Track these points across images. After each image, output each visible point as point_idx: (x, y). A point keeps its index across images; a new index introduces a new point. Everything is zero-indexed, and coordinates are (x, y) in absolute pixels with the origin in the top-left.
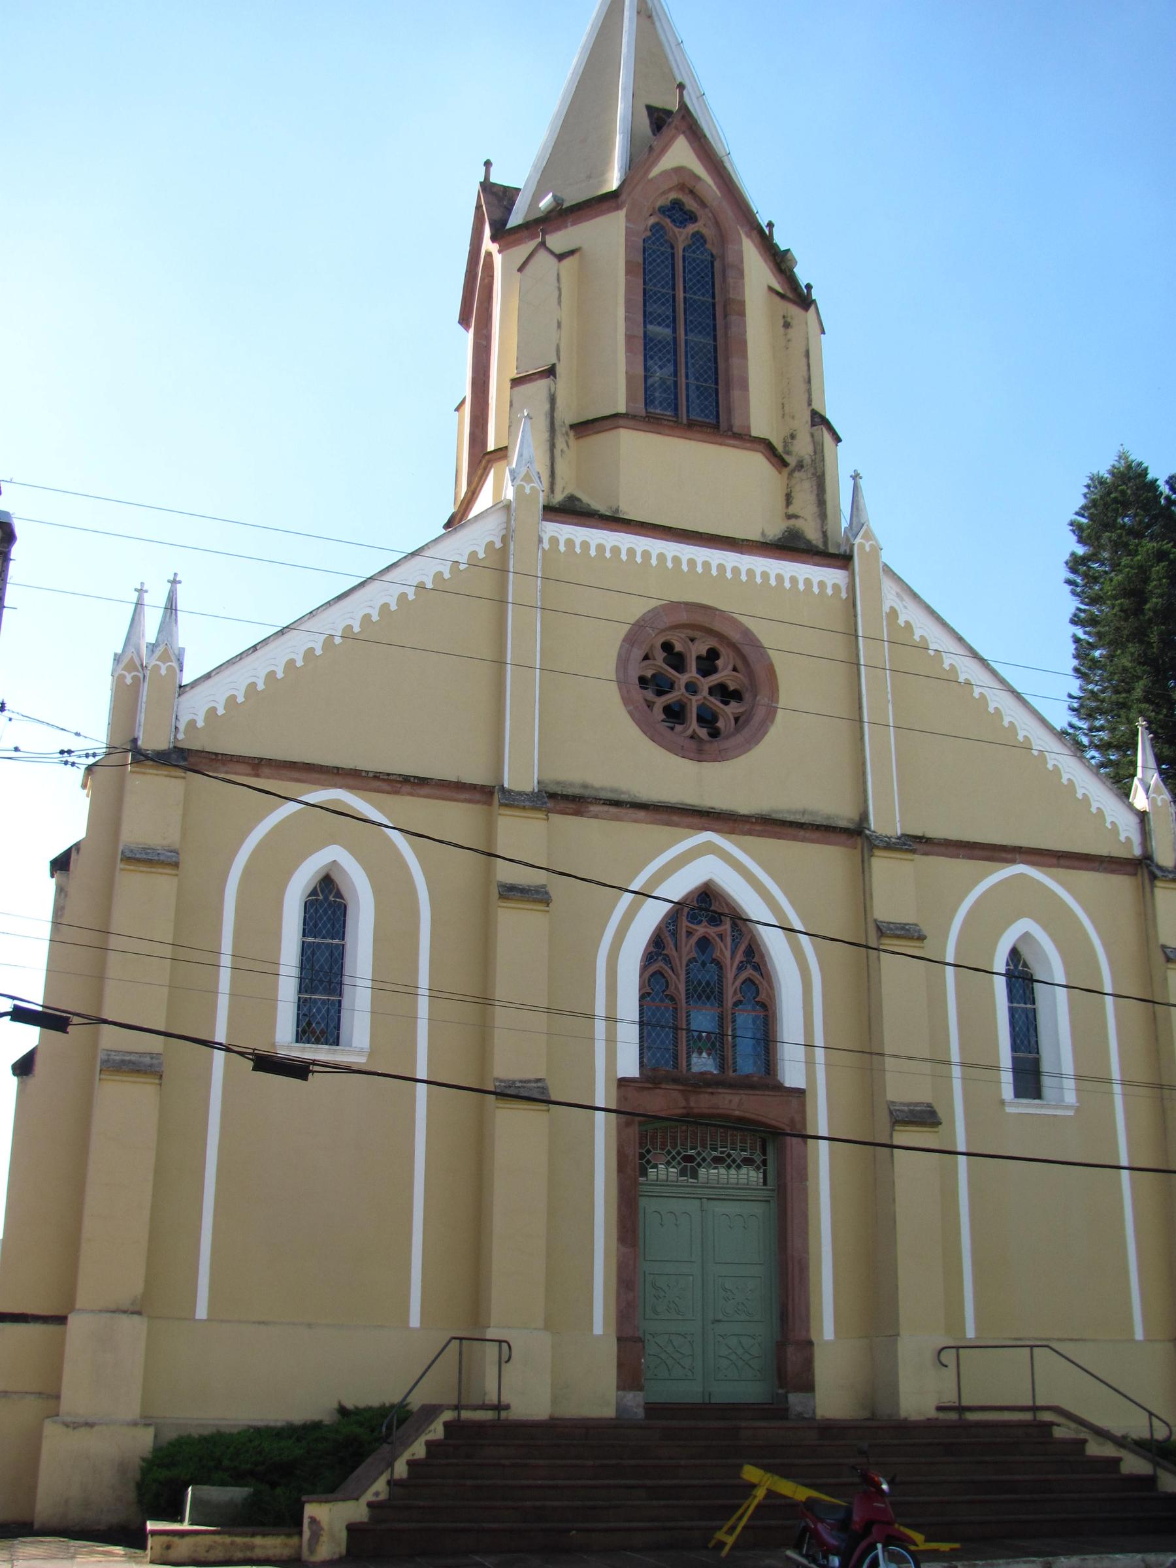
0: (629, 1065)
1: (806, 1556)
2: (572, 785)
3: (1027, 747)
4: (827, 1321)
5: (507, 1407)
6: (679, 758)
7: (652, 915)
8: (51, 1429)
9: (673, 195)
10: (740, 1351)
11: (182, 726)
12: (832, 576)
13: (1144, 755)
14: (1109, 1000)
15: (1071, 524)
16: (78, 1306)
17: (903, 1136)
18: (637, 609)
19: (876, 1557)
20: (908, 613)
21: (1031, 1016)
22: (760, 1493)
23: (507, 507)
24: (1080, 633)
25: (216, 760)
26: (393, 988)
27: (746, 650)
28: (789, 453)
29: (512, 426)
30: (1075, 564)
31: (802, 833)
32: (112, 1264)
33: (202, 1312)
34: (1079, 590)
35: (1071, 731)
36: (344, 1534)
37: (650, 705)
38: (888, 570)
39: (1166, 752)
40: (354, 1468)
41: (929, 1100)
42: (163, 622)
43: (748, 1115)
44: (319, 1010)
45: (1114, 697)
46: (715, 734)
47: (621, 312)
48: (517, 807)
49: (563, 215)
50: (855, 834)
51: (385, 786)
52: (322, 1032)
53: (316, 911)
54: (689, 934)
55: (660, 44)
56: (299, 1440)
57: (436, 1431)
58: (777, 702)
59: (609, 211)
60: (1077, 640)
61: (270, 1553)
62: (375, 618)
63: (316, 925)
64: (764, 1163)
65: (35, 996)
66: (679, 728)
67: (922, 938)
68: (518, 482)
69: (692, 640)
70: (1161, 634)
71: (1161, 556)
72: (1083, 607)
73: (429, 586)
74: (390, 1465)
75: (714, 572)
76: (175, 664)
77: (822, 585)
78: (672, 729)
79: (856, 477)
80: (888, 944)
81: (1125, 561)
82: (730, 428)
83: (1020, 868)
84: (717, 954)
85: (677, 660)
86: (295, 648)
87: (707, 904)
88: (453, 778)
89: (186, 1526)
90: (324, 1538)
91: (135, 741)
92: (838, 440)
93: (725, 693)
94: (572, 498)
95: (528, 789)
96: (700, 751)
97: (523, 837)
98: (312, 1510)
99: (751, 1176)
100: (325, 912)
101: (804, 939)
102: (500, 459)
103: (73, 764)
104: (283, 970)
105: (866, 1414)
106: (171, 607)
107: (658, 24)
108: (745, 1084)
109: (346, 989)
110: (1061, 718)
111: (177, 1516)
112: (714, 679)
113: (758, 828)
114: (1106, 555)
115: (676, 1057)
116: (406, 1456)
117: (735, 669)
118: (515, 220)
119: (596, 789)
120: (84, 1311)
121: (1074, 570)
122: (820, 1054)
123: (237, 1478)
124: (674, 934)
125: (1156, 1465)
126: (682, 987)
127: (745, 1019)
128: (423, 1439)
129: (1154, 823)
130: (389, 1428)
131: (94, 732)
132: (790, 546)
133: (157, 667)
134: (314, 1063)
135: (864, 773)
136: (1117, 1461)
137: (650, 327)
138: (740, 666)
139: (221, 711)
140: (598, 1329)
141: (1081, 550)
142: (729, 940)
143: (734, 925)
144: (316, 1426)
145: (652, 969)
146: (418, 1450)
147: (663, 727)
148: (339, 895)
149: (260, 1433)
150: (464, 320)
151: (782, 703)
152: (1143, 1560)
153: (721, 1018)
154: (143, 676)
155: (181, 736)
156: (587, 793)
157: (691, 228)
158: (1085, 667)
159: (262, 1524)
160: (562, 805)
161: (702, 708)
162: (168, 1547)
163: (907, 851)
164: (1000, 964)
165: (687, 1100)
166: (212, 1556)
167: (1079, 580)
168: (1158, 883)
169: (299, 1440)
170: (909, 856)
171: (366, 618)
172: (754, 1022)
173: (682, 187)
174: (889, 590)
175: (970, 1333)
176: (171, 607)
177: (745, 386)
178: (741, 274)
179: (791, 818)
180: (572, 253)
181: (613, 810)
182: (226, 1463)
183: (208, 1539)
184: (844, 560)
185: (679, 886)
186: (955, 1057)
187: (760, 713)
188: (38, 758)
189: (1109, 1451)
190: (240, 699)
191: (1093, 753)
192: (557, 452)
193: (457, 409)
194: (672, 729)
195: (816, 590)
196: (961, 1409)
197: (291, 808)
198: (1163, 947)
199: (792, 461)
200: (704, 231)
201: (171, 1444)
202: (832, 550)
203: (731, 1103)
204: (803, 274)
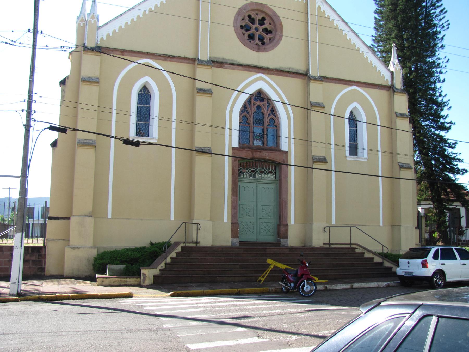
0: (236, 144)
1: (284, 284)
2: (219, 58)
4: (292, 219)
5: (199, 243)
6: (252, 51)
7: (243, 98)
8: (67, 249)
10: (267, 227)
11: (99, 39)
13: (394, 54)
14: (379, 127)
16: (74, 214)
17: (316, 166)
19: (304, 284)
21: (355, 131)
22: (272, 267)
24: (377, 16)
25: (110, 50)
26: (165, 119)
27: (274, 17)
31: (289, 74)
32: (83, 201)
33: (110, 216)
34: (377, 3)
35: (372, 47)
36: (153, 278)
39: (401, 54)
40: (155, 260)
41: (324, 155)
42: (92, 7)
43: (270, 159)
44: (143, 127)
45: (386, 37)
46: (263, 44)
48: (203, 65)
50: (305, 75)
51: (162, 58)
52: (144, 133)
53: (141, 96)
54: (254, 104)
56: (139, 252)
57: (179, 249)
60: (375, 18)
61: (132, 283)
62: (159, 6)
63: (141, 101)
64: (275, 173)
65: (57, 123)
66: (252, 41)
67: (324, 107)
70: (401, 17)
72: (378, 8)
74: (166, 259)
76: (96, 20)
78: (250, 42)
83: (354, 87)
84: (262, 110)
85: (252, 21)
87: (260, 96)
89: (107, 276)
90: (147, 279)
91: (84, 44)
93: (267, 31)
95: (206, 60)
96: (259, 49)
97: (204, 73)
98: (143, 271)
99: (271, 176)
100: (144, 97)
101: (289, 106)
103: (65, 51)
104: (132, 114)
105: (303, 245)
108: (270, 150)
109: (151, 120)
110: (369, 42)
111: (105, 273)
112: (264, 27)
113: (276, 73)
115: (249, 141)
116: (170, 256)
117: (270, 24)
119: (227, 60)
120: (75, 216)
122: (292, 141)
123: (122, 262)
124: (250, 104)
125: (383, 259)
126: (252, 120)
127: (271, 130)
128: (175, 251)
130: (165, 248)
131: (72, 41)
133: (90, 21)
134: (141, 142)
135: (308, 57)
136: (373, 258)
138: (272, 23)
139: (111, 35)
140: (226, 220)
142: (266, 107)
143: (268, 102)
144: (144, 248)
145: (243, 115)
146: (173, 254)
147: (248, 41)
148: (148, 91)
149: (128, 250)
151: (284, 34)
153: (263, 130)
154: (86, 24)
156: (224, 61)
158: (378, 27)
159: (129, 275)
160: (216, 65)
161: (260, 36)
162: (103, 281)
163: (321, 81)
164: (347, 115)
165: (253, 154)
166: (115, 284)
168: (395, 93)
169: (139, 252)
170: (321, 82)
172: (273, 131)
175: (334, 223)
179: (286, 70)
181: (232, 66)
182: (118, 258)
183: (114, 279)
185: (252, 90)
186: (332, 142)
187: (277, 37)
188: (54, 49)
189: (371, 256)
190: (117, 31)
191: (378, 53)
194: (250, 42)
196: (330, 244)
198: (396, 112)
201: (102, 253)
203: (266, 155)
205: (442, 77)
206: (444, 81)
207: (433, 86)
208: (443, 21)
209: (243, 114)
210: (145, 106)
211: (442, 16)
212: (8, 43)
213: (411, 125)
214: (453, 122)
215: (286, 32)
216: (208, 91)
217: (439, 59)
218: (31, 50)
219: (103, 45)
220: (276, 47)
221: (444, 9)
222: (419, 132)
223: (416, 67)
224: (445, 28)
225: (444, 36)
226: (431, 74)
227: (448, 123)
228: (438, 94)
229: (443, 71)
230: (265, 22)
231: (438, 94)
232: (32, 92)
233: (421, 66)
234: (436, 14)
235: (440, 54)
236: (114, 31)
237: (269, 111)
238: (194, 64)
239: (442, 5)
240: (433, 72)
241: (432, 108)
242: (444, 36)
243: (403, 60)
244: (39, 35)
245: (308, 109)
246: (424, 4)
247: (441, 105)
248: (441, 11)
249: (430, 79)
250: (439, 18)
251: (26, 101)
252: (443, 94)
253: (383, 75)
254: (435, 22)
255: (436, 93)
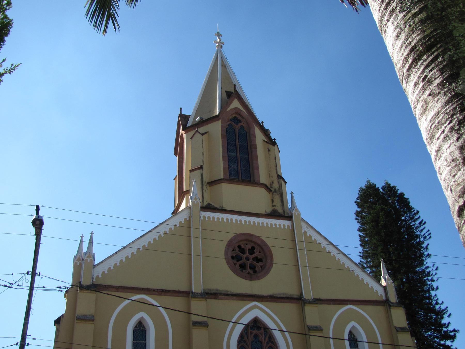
2: (213, 290)
3: (348, 269)
7: (239, 329)
9: (234, 116)
12: (287, 223)
15: (355, 202)
18: (230, 236)
20: (310, 232)
23: (190, 208)
28: (272, 187)
29: (191, 185)
30: (357, 213)
37: (235, 264)
38: (303, 220)
46: (255, 272)
47: (221, 150)
49: (203, 122)
50: (299, 300)
53: (137, 333)
54: (251, 333)
55: (228, 74)
58: (273, 261)
59: (216, 121)
60: (360, 236)
63: (137, 337)
66: (244, 271)
68: (193, 200)
69: (247, 244)
71: (382, 210)
73: (168, 232)
75: (252, 224)
76: (92, 259)
77: (284, 226)
78: (242, 271)
79: (292, 193)
80: (312, 333)
81: (372, 212)
82: (254, 181)
85: (242, 250)
86: (128, 252)
87: (256, 324)
88: (177, 290)
91: (80, 282)
92: (286, 183)
93: (258, 260)
94: (209, 204)
95: (200, 292)
97: (199, 307)
101: (287, 334)
102: (187, 194)
103: (61, 291)
106: (91, 242)
107: (228, 69)
110: (357, 259)
112: (254, 256)
114: (366, 210)
117: (260, 252)
118: (189, 124)
121: (357, 215)
124: (247, 334)
129: (388, 289)
131: (68, 281)
132: (274, 215)
133: (87, 260)
137: (229, 153)
141: (359, 210)
145: (240, 345)
148: (144, 327)
150: (175, 154)
151: (274, 262)
152: (429, 144)
154: (83, 262)
155: (94, 280)
157: (240, 124)
158: (363, 244)
161: (251, 264)
164: (346, 337)
167: (359, 218)
171: (149, 243)
173: (236, 113)
174: (304, 225)
176: (91, 242)
177: (258, 169)
178: (255, 137)
179: (280, 296)
180: (206, 133)
181: (226, 297)
184: (290, 218)
185: (246, 319)
188: (50, 289)
190: (112, 268)
191: (368, 269)
192: (204, 191)
193: (174, 179)
194: (242, 271)
195: (282, 227)
197: (127, 302)
198: (395, 327)
199: (273, 190)
200: (244, 125)
202: (286, 215)
204: (273, 136)
205: (435, 285)
206: (437, 288)
207: (427, 295)
208: (424, 231)
209: (241, 345)
210: (141, 342)
211: (422, 227)
212: (6, 286)
213: (414, 338)
214: (456, 329)
215: (276, 259)
216: (204, 323)
217: (428, 267)
218: (27, 292)
219: (99, 283)
220: (268, 274)
221: (423, 220)
222: (423, 344)
223: (407, 278)
224: (428, 237)
225: (428, 245)
226: (424, 283)
227: (451, 332)
228: (434, 302)
229: (435, 279)
230: (255, 251)
231: (434, 302)
232: (26, 334)
233: (411, 276)
234: (416, 226)
235: (429, 262)
236: (110, 269)
237: (267, 339)
238: (189, 297)
239: (419, 217)
240: (425, 280)
241: (431, 317)
242: (428, 245)
243: (393, 274)
244: (37, 277)
245: (306, 335)
246: (403, 218)
247: (441, 313)
248: (420, 223)
249: (423, 289)
250: (420, 229)
251: (19, 344)
252: (440, 302)
253: (376, 290)
254: (417, 233)
255: (432, 302)
